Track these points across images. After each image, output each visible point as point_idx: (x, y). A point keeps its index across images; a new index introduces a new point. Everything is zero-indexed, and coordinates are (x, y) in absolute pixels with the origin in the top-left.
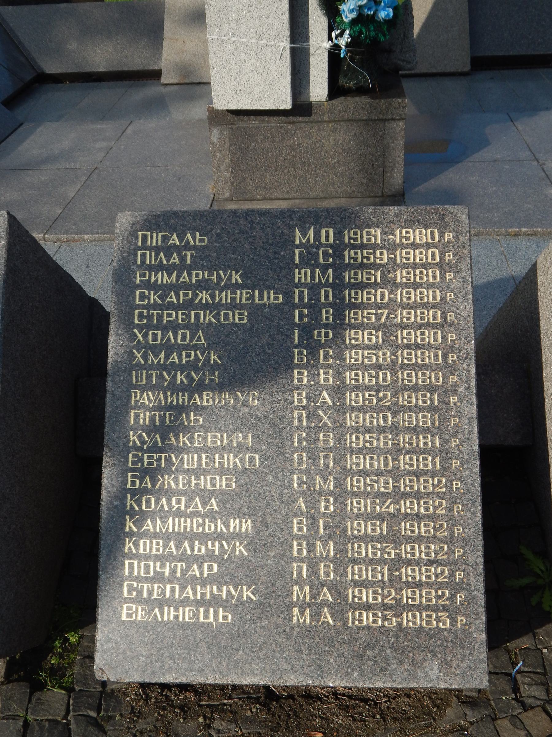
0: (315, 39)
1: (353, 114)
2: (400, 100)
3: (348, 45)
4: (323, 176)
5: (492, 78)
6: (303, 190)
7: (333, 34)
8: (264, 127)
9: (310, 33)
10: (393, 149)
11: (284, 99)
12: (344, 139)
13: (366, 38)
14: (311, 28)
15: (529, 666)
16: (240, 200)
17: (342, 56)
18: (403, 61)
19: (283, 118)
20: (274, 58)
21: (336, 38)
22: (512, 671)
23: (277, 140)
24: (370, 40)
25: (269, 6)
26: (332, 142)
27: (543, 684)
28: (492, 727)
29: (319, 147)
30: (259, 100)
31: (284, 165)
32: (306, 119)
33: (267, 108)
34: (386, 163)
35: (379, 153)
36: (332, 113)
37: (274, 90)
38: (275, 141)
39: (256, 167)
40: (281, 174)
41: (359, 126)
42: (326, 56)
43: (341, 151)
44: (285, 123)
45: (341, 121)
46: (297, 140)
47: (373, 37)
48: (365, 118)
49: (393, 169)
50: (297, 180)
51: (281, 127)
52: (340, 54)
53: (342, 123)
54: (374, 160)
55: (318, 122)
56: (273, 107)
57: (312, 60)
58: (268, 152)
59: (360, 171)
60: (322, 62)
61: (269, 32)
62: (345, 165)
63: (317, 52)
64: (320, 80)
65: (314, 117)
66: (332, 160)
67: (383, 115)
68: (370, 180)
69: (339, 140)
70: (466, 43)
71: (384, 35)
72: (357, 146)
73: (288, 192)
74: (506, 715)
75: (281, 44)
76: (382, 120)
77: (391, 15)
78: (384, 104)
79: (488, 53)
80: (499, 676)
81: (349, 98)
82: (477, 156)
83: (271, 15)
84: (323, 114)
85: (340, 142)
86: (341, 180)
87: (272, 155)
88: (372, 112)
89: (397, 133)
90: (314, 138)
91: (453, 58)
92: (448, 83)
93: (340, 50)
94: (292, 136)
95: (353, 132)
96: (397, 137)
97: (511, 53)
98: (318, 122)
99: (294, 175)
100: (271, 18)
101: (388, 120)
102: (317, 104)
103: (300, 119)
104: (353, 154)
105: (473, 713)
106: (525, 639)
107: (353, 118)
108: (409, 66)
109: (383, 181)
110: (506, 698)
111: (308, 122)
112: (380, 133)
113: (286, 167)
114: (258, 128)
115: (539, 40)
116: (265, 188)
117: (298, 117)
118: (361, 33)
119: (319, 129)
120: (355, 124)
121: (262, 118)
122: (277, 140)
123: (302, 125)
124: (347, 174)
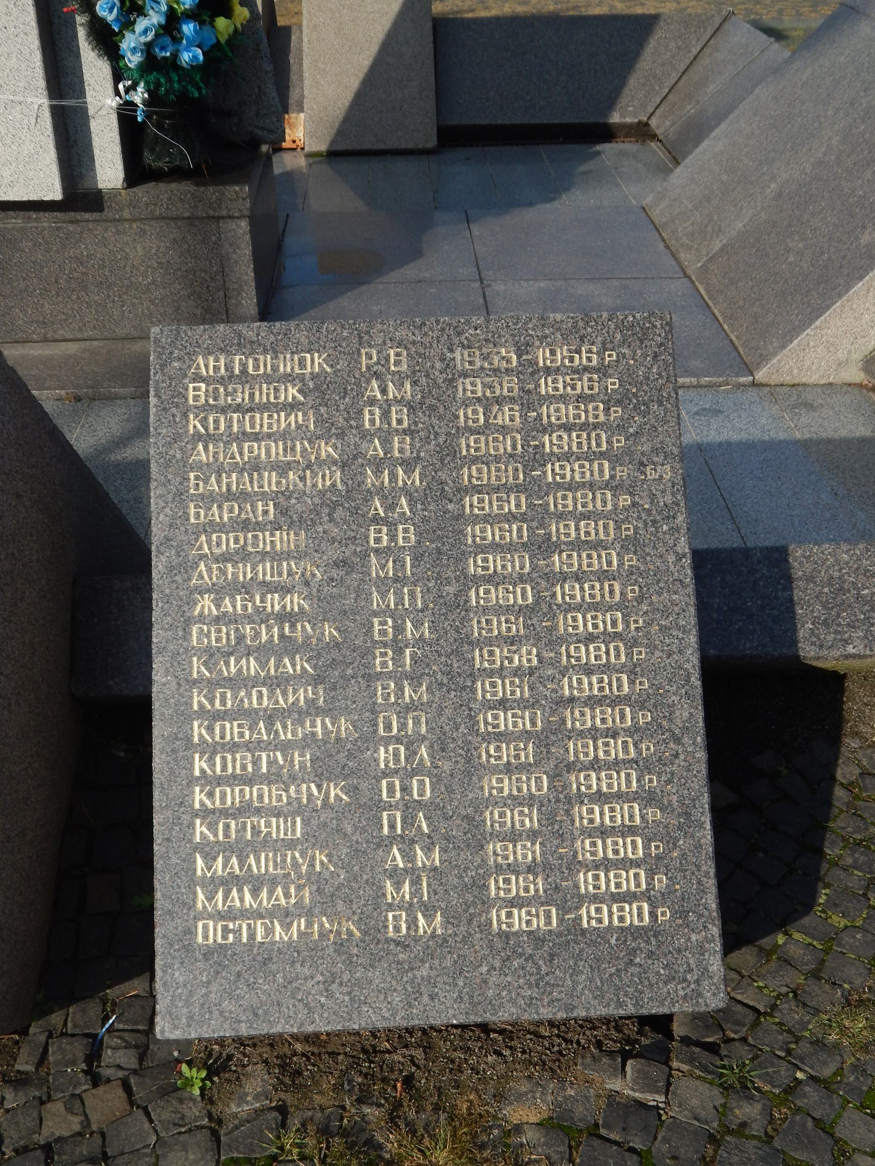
0: (94, 94)
1: (168, 208)
2: (237, 188)
3: (145, 102)
4: (133, 304)
5: (468, 159)
6: (104, 327)
7: (121, 87)
8: (31, 228)
9: (86, 84)
10: (236, 262)
11: (50, 184)
12: (159, 247)
13: (167, 92)
14: (87, 76)
15: (127, 1022)
16: (7, 342)
17: (139, 119)
18: (263, 129)
19: (59, 215)
20: (26, 121)
21: (127, 92)
22: (99, 1031)
23: (54, 248)
24: (176, 96)
25: (9, 42)
26: (140, 251)
27: (137, 1047)
28: (35, 1114)
29: (120, 259)
30: (11, 185)
31: (69, 288)
32: (95, 216)
33: (25, 199)
34: (227, 284)
35: (215, 269)
36: (134, 207)
37: (33, 172)
38: (51, 249)
39: (25, 290)
40: (67, 302)
41: (179, 228)
42: (114, 119)
43: (155, 265)
44: (64, 222)
45: (152, 219)
46: (86, 248)
47: (178, 91)
48: (186, 214)
49: (239, 293)
50: (94, 311)
51: (58, 229)
52: (136, 117)
53: (152, 223)
54: (208, 279)
55: (115, 220)
56: (33, 197)
57: (94, 125)
58: (42, 267)
59: (189, 297)
60: (109, 128)
61: (14, 82)
62: (164, 288)
63: (100, 113)
64: (110, 156)
65: (107, 213)
66: (143, 280)
67: (214, 210)
68: (206, 310)
69: (151, 248)
70: (430, 105)
71: (199, 89)
72: (180, 257)
73: (80, 329)
74: (62, 1095)
75: (35, 100)
76: (214, 217)
77: (201, 58)
78: (214, 194)
79: (466, 121)
80: (74, 1039)
81: (161, 185)
82: (394, 275)
83: (14, 55)
84: (122, 209)
85: (153, 251)
86: (162, 310)
87: (50, 272)
88: (196, 206)
89: (239, 238)
90: (112, 245)
91: (411, 128)
92: (400, 166)
93: (136, 111)
94: (77, 242)
95: (172, 236)
96: (240, 244)
97: (500, 122)
98: (115, 220)
99: (87, 302)
100: (14, 60)
101: (223, 218)
102: (111, 193)
103: (87, 216)
104: (175, 270)
105: (16, 1096)
106: (136, 982)
107: (169, 215)
108: (272, 137)
109: (227, 311)
110: (72, 1070)
111: (98, 220)
112: (213, 238)
113: (73, 290)
114: (22, 229)
115: (542, 103)
116: (44, 323)
117: (83, 214)
118: (158, 85)
119: (118, 232)
120: (173, 225)
121: (27, 214)
122: (54, 248)
123: (91, 226)
124: (169, 300)
